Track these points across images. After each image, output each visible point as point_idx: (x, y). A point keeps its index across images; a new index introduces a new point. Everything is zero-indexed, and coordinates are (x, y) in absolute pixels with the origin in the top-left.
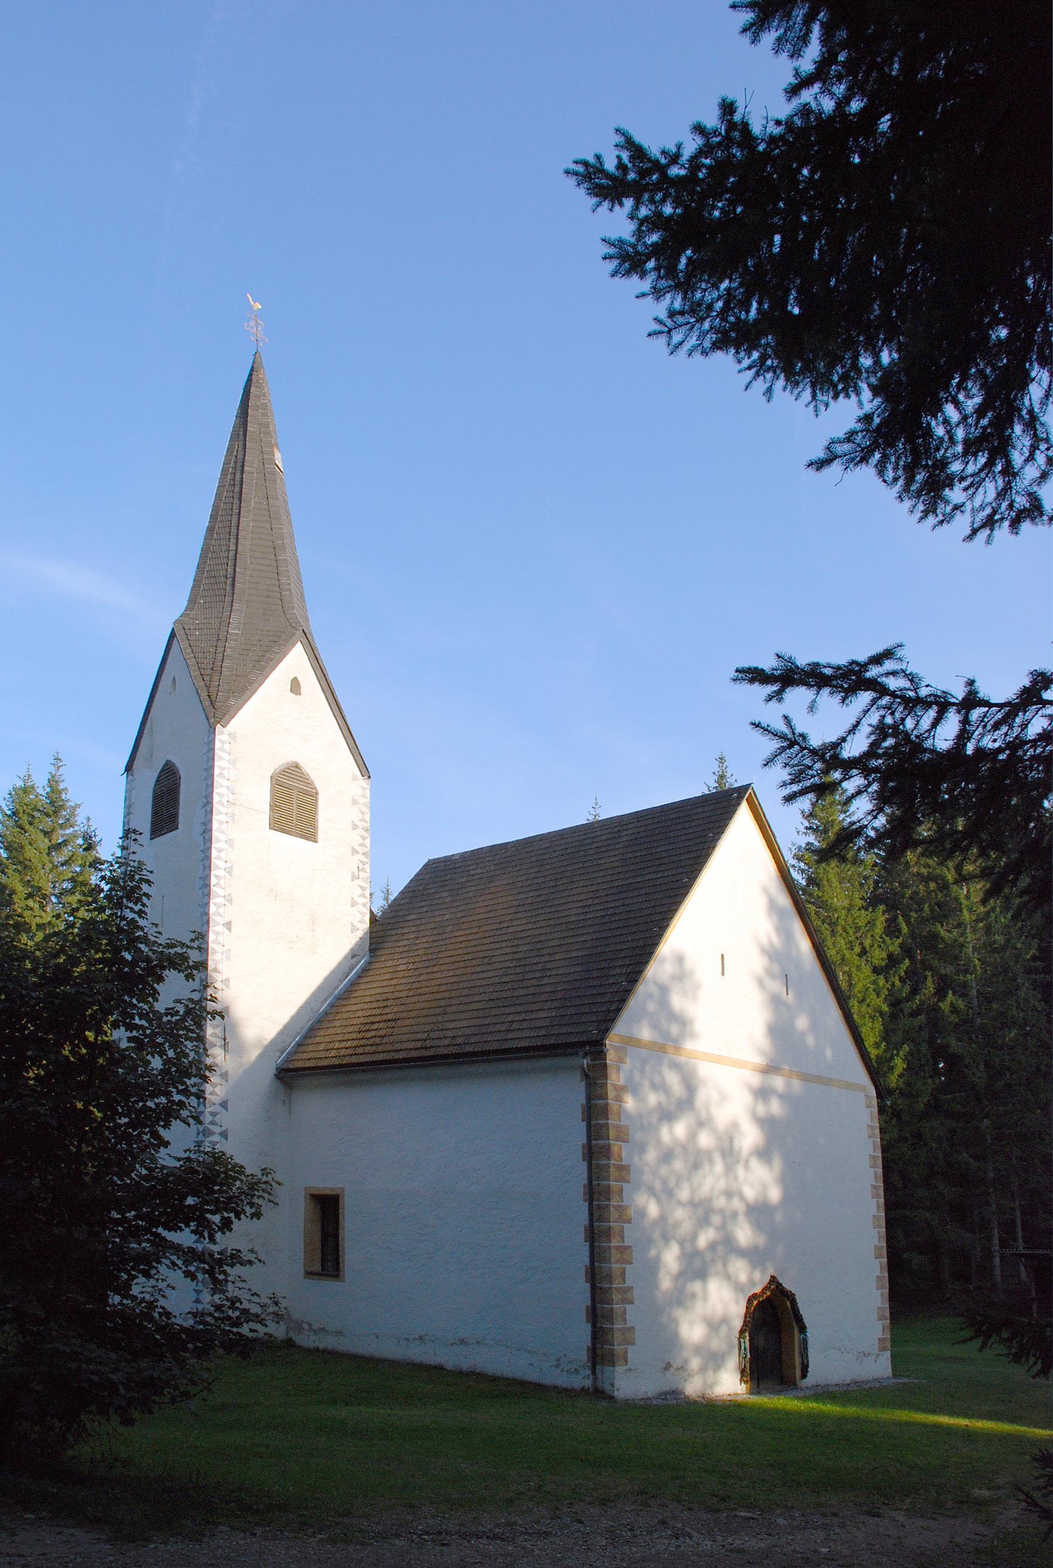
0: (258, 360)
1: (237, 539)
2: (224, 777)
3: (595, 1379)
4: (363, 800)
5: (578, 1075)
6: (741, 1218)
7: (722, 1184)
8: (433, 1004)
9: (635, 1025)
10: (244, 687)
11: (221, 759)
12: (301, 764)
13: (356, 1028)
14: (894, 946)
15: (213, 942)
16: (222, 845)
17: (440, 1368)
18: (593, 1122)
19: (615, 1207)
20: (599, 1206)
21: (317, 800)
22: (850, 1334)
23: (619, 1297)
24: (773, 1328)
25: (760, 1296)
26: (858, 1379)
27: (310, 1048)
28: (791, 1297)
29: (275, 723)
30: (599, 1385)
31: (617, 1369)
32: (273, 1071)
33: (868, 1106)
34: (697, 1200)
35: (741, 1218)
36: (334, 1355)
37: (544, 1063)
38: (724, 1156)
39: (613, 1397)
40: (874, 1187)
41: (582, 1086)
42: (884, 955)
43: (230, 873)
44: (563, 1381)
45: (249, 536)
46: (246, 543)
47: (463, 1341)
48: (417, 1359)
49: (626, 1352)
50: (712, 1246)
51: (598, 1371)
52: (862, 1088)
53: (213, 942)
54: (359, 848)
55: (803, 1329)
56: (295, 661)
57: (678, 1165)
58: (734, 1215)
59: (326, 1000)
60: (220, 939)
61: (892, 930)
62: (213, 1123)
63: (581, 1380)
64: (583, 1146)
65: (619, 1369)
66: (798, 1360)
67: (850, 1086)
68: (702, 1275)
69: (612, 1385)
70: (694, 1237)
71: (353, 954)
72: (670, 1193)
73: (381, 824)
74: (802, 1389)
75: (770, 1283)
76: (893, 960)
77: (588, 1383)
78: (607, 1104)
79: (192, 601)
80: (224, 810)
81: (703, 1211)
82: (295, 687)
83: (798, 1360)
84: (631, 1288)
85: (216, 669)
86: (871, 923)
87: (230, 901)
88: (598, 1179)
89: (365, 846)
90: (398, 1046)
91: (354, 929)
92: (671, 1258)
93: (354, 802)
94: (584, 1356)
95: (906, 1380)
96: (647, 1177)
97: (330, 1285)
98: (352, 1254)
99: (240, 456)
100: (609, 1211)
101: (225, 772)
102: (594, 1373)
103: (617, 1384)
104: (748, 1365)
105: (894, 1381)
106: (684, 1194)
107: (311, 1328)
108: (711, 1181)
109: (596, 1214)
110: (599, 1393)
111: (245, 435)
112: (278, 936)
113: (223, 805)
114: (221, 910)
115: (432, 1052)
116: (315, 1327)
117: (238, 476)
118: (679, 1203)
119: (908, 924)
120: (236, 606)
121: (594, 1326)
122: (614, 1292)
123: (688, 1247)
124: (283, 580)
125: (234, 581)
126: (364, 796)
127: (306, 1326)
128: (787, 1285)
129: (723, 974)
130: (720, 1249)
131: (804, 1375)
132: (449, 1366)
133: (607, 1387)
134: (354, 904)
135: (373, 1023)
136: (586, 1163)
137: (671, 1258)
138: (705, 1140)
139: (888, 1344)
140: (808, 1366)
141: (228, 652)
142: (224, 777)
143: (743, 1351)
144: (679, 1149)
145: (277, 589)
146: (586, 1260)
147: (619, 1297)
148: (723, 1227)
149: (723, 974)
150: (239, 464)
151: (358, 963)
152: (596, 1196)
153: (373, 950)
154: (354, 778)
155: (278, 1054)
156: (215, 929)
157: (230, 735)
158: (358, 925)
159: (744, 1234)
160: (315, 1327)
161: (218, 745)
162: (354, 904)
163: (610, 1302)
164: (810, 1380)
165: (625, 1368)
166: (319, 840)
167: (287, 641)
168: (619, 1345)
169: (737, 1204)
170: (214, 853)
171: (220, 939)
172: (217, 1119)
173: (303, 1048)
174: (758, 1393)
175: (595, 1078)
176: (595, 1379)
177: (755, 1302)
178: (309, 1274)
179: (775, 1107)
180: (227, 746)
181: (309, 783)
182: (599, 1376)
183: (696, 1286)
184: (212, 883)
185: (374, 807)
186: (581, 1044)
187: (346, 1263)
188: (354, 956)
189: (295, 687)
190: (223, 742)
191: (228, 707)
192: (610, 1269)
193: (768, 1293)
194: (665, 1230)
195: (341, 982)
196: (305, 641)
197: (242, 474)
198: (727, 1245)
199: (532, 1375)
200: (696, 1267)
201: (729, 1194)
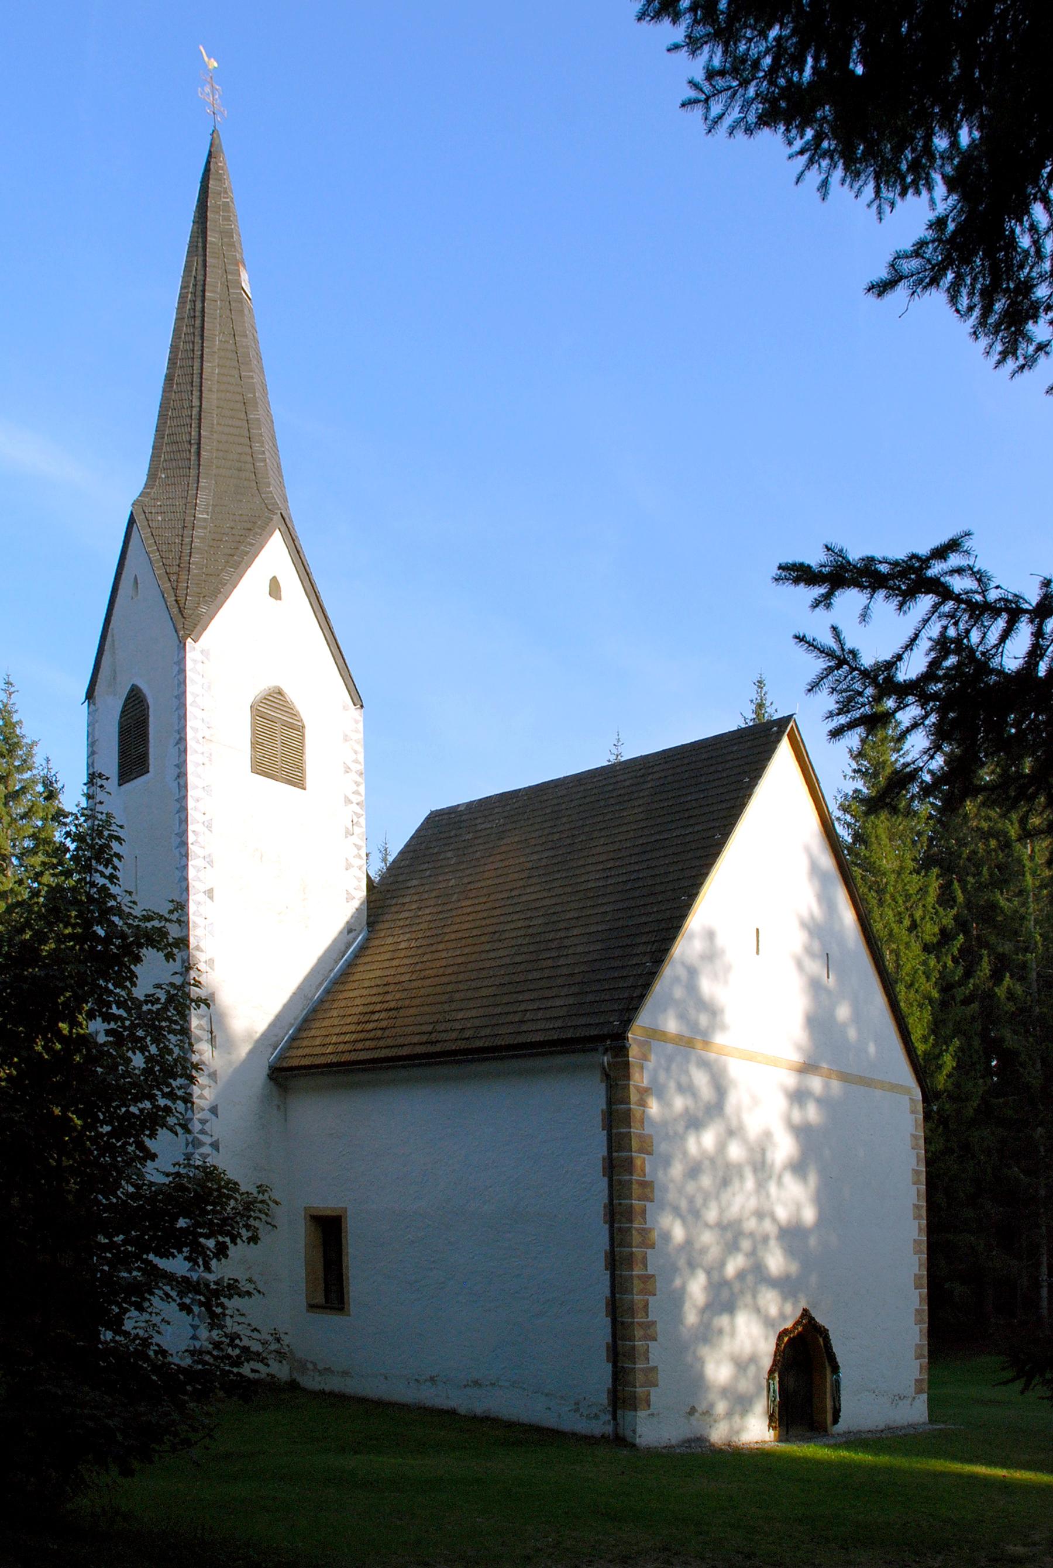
0: (217, 142)
2: (198, 706)
3: (616, 1425)
5: (598, 1076)
6: (773, 1243)
7: (752, 1203)
10: (217, 590)
12: (286, 690)
14: (948, 919)
17: (452, 1413)
18: (614, 1131)
19: (637, 1230)
20: (620, 1229)
22: (885, 1376)
23: (642, 1333)
24: (804, 1366)
26: (892, 1425)
28: (824, 1333)
30: (620, 1432)
31: (639, 1413)
32: (265, 1071)
33: (913, 1112)
34: (725, 1222)
35: (773, 1243)
37: (559, 1060)
38: (755, 1171)
39: (634, 1445)
40: (916, 1172)
41: (601, 1089)
42: (936, 930)
44: (583, 1427)
45: (215, 388)
47: (476, 1383)
52: (906, 1090)
55: (835, 1369)
57: (706, 1181)
58: (765, 1239)
61: (946, 899)
63: (601, 1427)
64: (604, 1159)
65: (642, 1414)
67: (894, 1088)
68: (730, 1308)
69: (634, 1431)
70: (722, 1264)
72: (696, 1214)
73: (378, 767)
74: (833, 1436)
75: (803, 1316)
76: (946, 936)
78: (629, 1110)
79: (152, 475)
81: (732, 1234)
82: (275, 589)
84: (654, 1323)
86: (923, 890)
87: (211, 863)
90: (401, 1041)
91: (350, 898)
92: (697, 1288)
93: (346, 738)
94: (604, 1399)
95: (943, 1426)
96: (672, 1196)
97: (334, 1319)
99: (200, 277)
100: (631, 1235)
102: (615, 1418)
103: (639, 1430)
104: (777, 1409)
105: (930, 1426)
106: (712, 1215)
108: (741, 1200)
109: (617, 1238)
110: (620, 1441)
111: (205, 248)
115: (438, 1048)
117: (199, 305)
118: (707, 1225)
119: (964, 890)
120: (203, 482)
122: (636, 1327)
123: (716, 1276)
124: (256, 446)
127: (310, 1366)
128: (820, 1320)
130: (750, 1279)
131: (836, 1421)
132: (462, 1411)
133: (628, 1433)
136: (606, 1179)
137: (697, 1288)
138: (735, 1152)
139: (925, 1386)
140: (840, 1410)
141: (197, 543)
143: (772, 1394)
144: (707, 1163)
145: (249, 459)
146: (607, 1292)
150: (200, 283)
151: (355, 939)
152: (617, 1217)
153: (371, 924)
155: (270, 1050)
157: (202, 652)
159: (775, 1262)
163: (632, 1338)
164: (842, 1426)
165: (649, 1412)
167: (263, 529)
169: (768, 1226)
172: (207, 1127)
175: (616, 1078)
176: (616, 1425)
177: (786, 1339)
179: (812, 1113)
181: (295, 715)
182: (620, 1421)
183: (724, 1320)
186: (601, 1038)
187: (351, 1294)
188: (350, 931)
189: (275, 589)
191: (199, 615)
193: (800, 1329)
196: (284, 528)
197: (203, 301)
198: (757, 1272)
199: (550, 1421)
200: (724, 1300)
201: (760, 1215)
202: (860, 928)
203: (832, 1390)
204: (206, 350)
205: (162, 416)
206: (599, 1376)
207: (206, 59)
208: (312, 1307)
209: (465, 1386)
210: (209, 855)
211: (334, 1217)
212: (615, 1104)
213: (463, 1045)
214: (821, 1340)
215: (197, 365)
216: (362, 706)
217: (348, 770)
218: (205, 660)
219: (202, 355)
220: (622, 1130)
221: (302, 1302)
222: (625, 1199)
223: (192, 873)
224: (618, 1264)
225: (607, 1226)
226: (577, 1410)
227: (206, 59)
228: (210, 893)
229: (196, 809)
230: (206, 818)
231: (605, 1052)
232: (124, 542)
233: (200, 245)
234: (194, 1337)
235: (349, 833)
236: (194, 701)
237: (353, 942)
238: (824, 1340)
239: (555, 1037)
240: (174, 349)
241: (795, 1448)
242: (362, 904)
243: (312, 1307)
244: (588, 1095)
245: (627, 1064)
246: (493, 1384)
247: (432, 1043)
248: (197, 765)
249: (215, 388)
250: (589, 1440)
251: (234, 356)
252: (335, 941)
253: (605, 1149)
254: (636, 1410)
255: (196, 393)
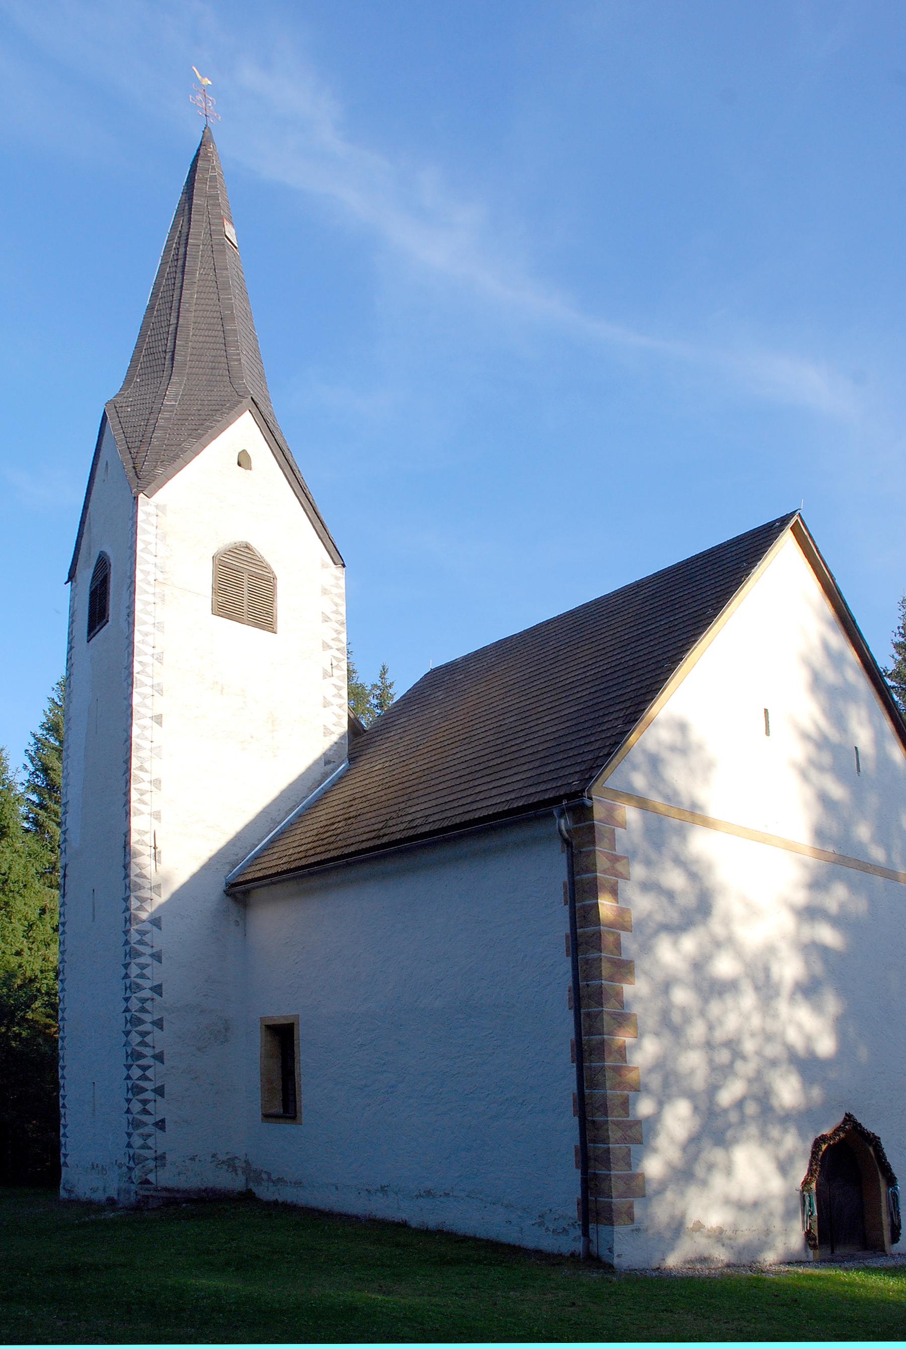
0: (208, 134)
1: (179, 312)
2: (150, 553)
4: (335, 591)
5: (558, 846)
7: (756, 1021)
8: (400, 793)
9: (629, 772)
10: (176, 456)
11: (145, 532)
12: (254, 544)
13: (315, 832)
15: (138, 737)
16: (148, 628)
17: (403, 1226)
19: (609, 1014)
20: (588, 1015)
21: (274, 586)
23: (619, 1134)
25: (831, 1138)
27: (265, 859)
28: (874, 1141)
29: (217, 498)
30: (593, 1248)
31: (617, 1228)
32: (223, 887)
36: (289, 1208)
39: (611, 1266)
41: (562, 861)
43: (160, 659)
44: (549, 1244)
45: (193, 309)
46: (189, 317)
47: (429, 1193)
48: (380, 1215)
49: (631, 1207)
50: (740, 1104)
51: (591, 1231)
53: (138, 737)
54: (332, 643)
55: (891, 1181)
56: (244, 431)
59: (292, 810)
60: (147, 733)
62: (141, 942)
63: (571, 1243)
64: (567, 937)
65: (620, 1230)
66: (885, 1220)
69: (611, 1250)
71: (327, 760)
73: (362, 619)
74: (893, 1256)
75: (845, 1122)
77: (579, 1247)
78: (596, 878)
79: (128, 381)
80: (151, 589)
81: (726, 1054)
82: (244, 461)
83: (885, 1220)
85: (145, 440)
87: (161, 692)
88: (586, 978)
89: (340, 641)
90: (349, 841)
91: (327, 732)
92: (677, 1121)
93: (325, 592)
94: (573, 1212)
97: (287, 1128)
98: (310, 1091)
99: (185, 230)
101: (152, 548)
102: (586, 1233)
103: (617, 1249)
106: (697, 1031)
107: (269, 1179)
110: (593, 1260)
111: (190, 209)
112: (229, 738)
113: (149, 583)
114: (148, 702)
115: (385, 840)
116: (274, 1177)
117: (182, 250)
120: (174, 379)
121: (584, 1172)
122: (611, 1127)
124: (232, 350)
125: (173, 356)
126: (337, 586)
127: (264, 1176)
128: (870, 1127)
129: (767, 733)
132: (414, 1224)
133: (604, 1252)
134: (326, 704)
135: (333, 824)
137: (677, 1121)
140: (900, 1227)
141: (161, 422)
142: (150, 553)
143: (807, 1208)
145: (224, 360)
147: (619, 1134)
148: (757, 1078)
149: (767, 733)
150: (184, 235)
151: (334, 770)
152: (584, 1002)
153: (353, 758)
154: (324, 566)
155: (228, 867)
156: (141, 722)
157: (157, 507)
158: (333, 729)
160: (274, 1177)
161: (141, 516)
162: (326, 704)
163: (606, 1140)
166: (279, 630)
167: (231, 409)
168: (620, 1197)
170: (137, 637)
171: (147, 733)
172: (147, 938)
173: (258, 861)
174: (831, 1261)
177: (824, 1147)
178: (267, 1116)
180: (153, 519)
181: (267, 567)
182: (593, 1237)
183: (717, 1155)
184: (135, 671)
185: (351, 598)
186: (556, 800)
187: (303, 1102)
188: (327, 763)
189: (244, 461)
190: (148, 514)
191: (154, 476)
192: (604, 1097)
194: (670, 1084)
195: (311, 790)
196: (255, 410)
197: (186, 247)
199: (510, 1236)
200: (715, 1130)
202: (894, 729)
203: (889, 1206)
204: (185, 282)
205: (142, 336)
206: (568, 1184)
207: (199, 77)
208: (268, 1116)
209: (417, 1197)
210: (158, 684)
211: (288, 1024)
212: (579, 873)
213: (411, 833)
214: (871, 1149)
215: (176, 293)
216: (344, 566)
217: (326, 619)
218: (160, 514)
219: (182, 286)
220: (587, 902)
221: (257, 1109)
222: (594, 979)
223: (136, 699)
224: (586, 1055)
225: (572, 1012)
226: (541, 1224)
227: (199, 77)
228: (158, 719)
229: (143, 642)
230: (156, 651)
231: (561, 815)
232: (99, 436)
233: (187, 208)
234: (129, 1145)
235: (326, 675)
236: (146, 548)
237: (331, 773)
238: (875, 1150)
239: (506, 808)
240: (157, 285)
241: (841, 1272)
242: (342, 738)
243: (268, 1116)
244: (547, 868)
245: (592, 828)
246: (447, 1195)
247: (379, 837)
248: (147, 603)
249: (193, 309)
250: (553, 1260)
251: (214, 284)
252: (309, 769)
253: (568, 926)
254: (613, 1225)
255: (174, 314)
